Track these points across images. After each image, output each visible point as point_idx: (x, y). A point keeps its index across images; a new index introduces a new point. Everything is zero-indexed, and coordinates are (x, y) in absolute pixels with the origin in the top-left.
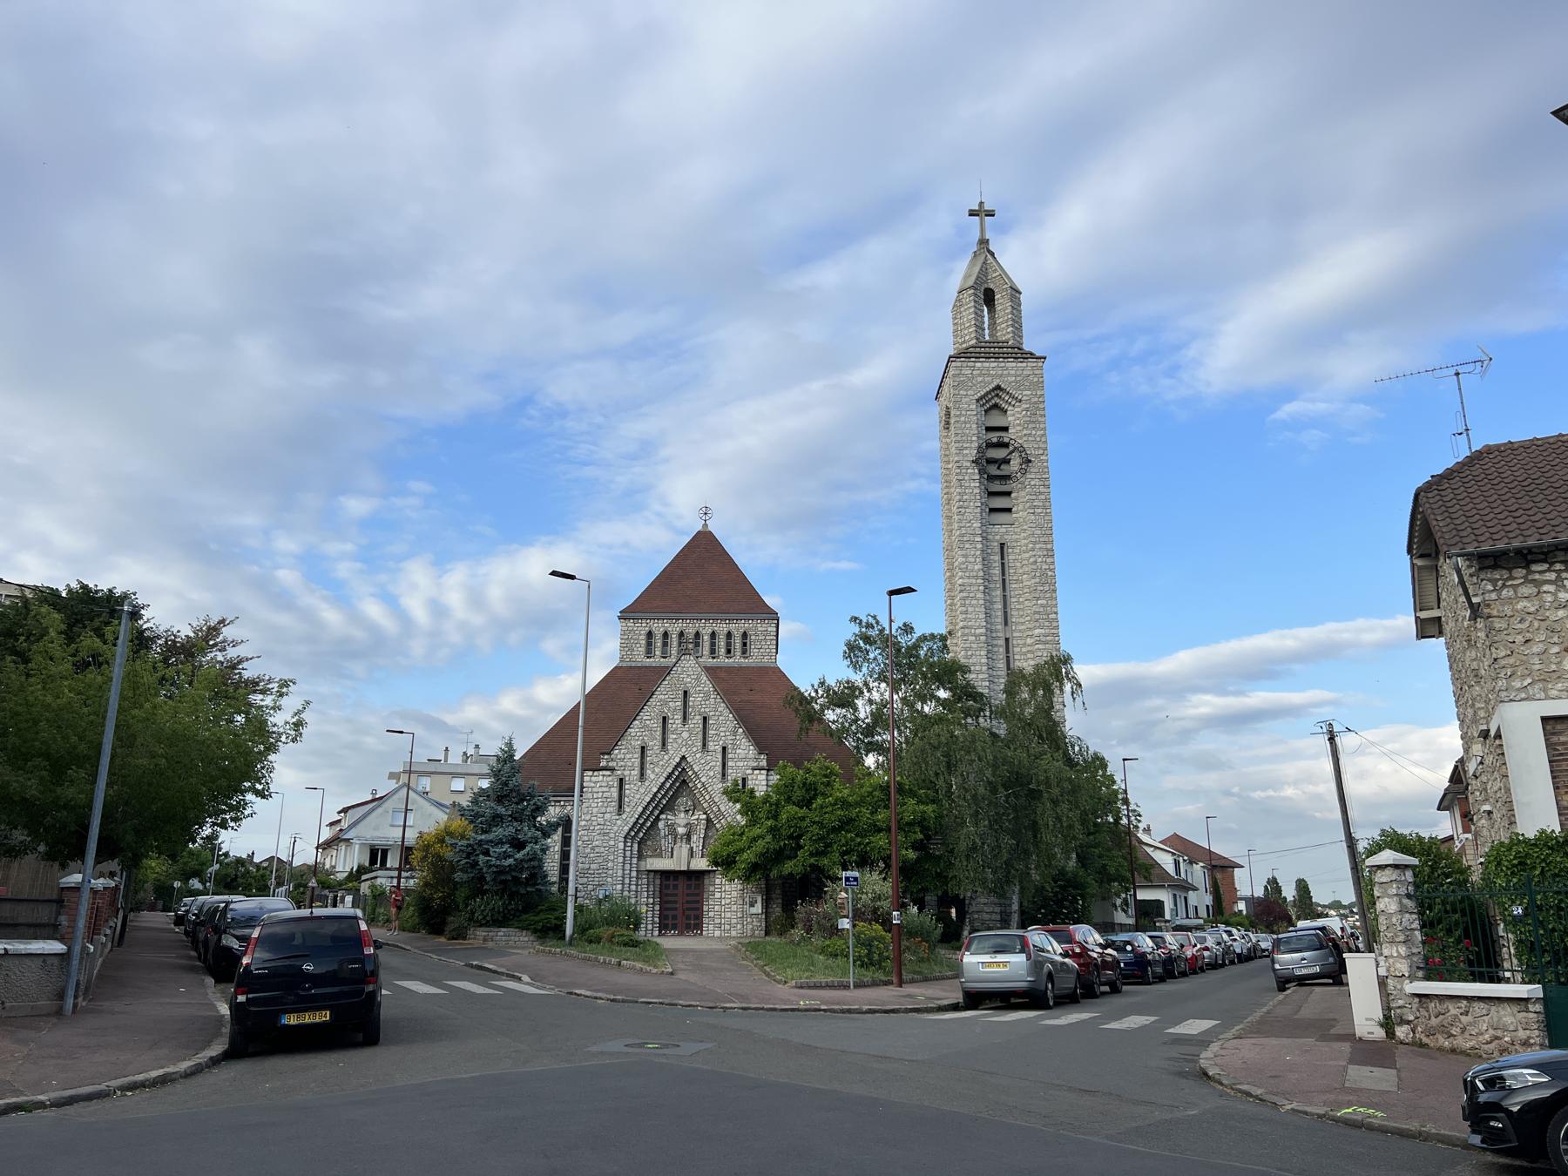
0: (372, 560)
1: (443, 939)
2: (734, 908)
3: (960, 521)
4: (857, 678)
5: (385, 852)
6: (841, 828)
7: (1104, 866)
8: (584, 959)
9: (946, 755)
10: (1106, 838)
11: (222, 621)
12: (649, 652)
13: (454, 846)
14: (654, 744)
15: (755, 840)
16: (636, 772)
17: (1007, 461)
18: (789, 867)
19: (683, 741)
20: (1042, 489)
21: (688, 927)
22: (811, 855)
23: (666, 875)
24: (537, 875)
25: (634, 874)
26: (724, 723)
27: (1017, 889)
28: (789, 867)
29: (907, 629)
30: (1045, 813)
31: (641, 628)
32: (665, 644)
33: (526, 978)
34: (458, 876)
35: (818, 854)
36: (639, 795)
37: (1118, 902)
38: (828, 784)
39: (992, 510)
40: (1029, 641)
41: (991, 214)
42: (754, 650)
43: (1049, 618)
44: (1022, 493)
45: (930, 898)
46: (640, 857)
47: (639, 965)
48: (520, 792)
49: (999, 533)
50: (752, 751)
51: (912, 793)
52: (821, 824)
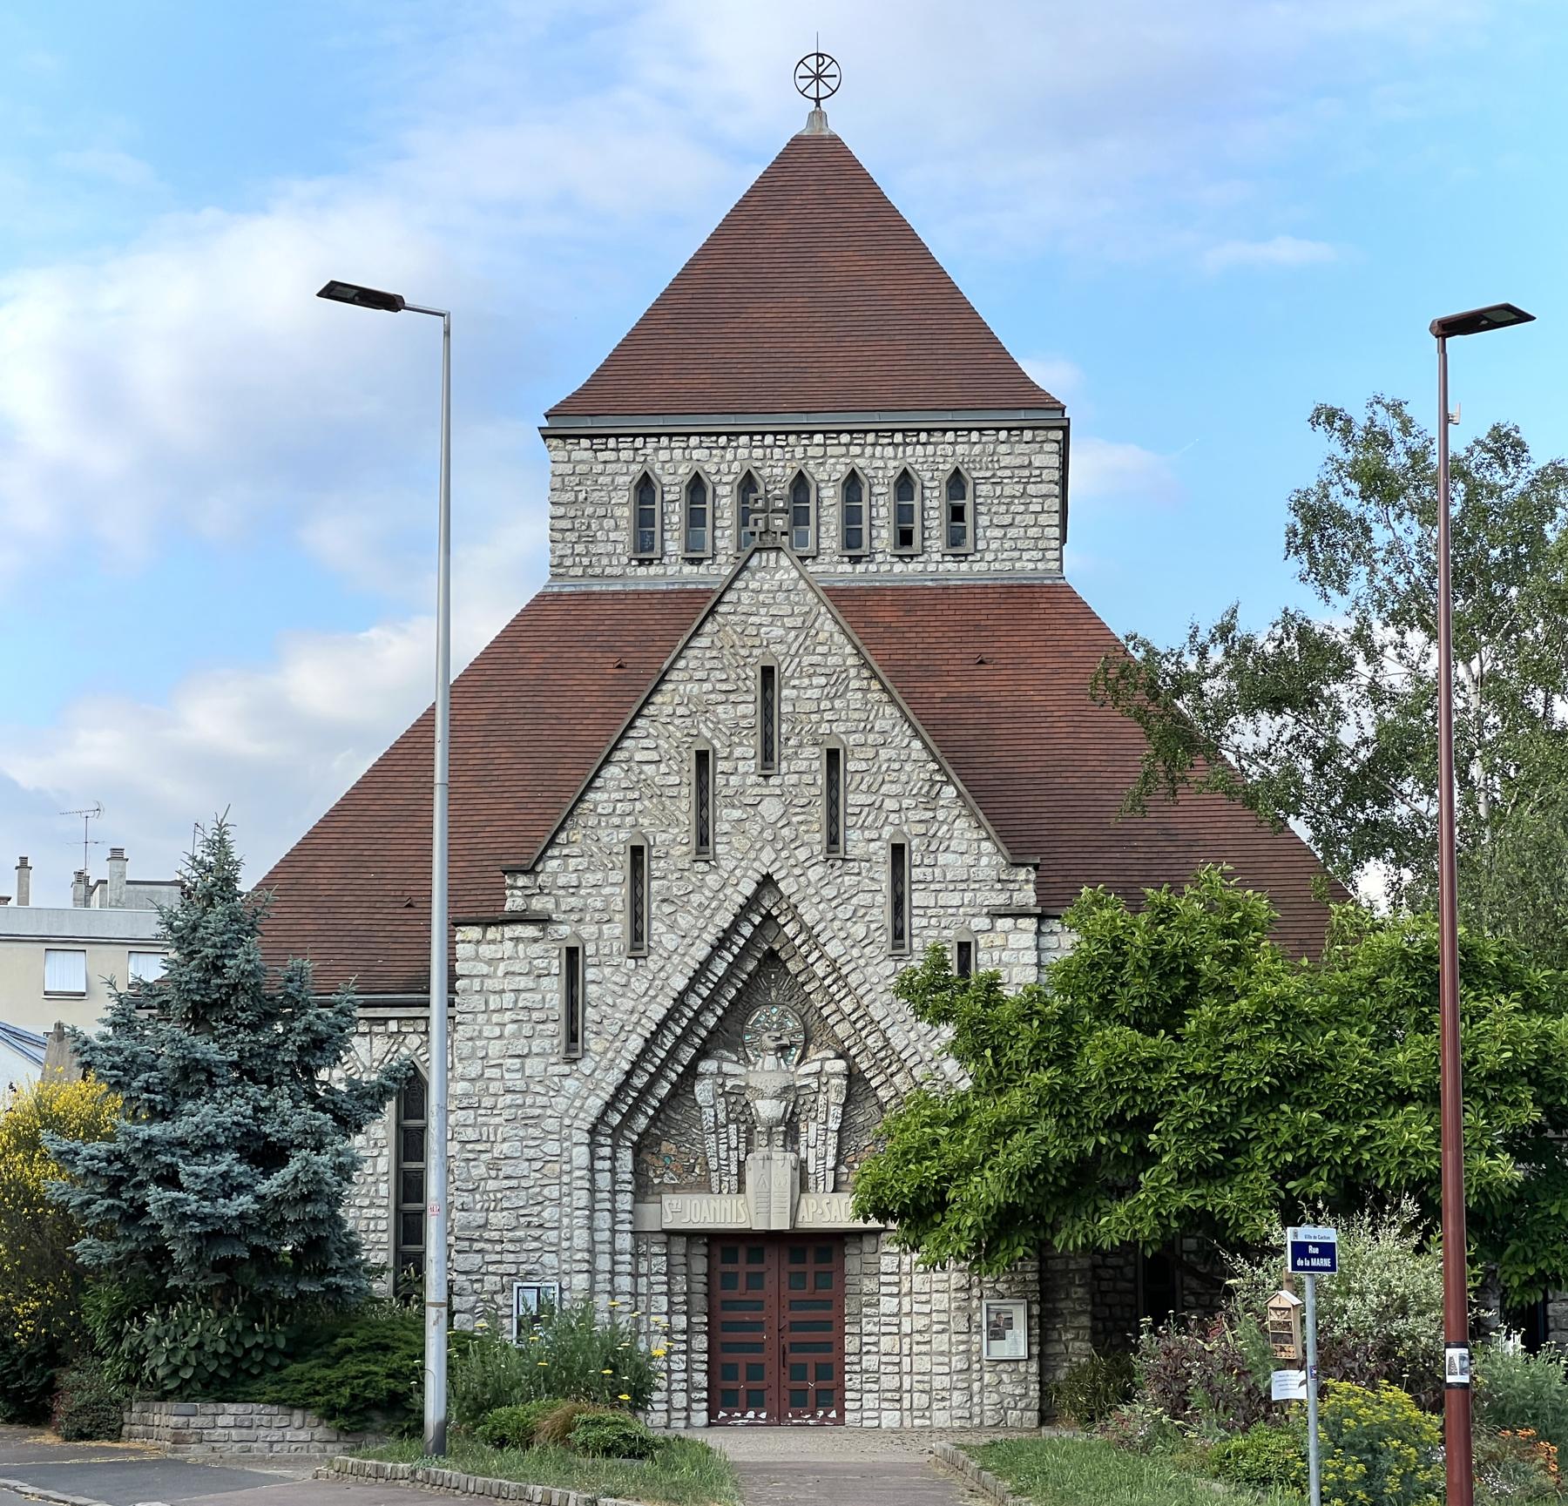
14: (672, 841)
29: (1505, 446)
42: (986, 530)
51: (1506, 980)
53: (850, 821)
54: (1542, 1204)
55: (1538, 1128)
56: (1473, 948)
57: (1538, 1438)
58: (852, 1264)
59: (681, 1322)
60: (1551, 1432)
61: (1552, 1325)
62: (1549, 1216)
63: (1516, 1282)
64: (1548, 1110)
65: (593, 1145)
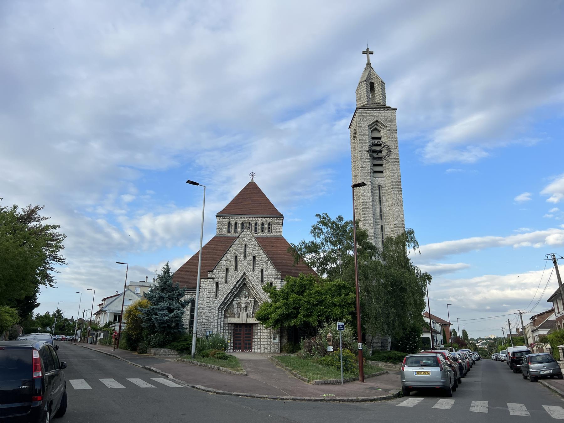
0: (131, 216)
1: (136, 353)
2: (266, 340)
3: (362, 176)
4: (318, 241)
5: (120, 317)
6: (318, 304)
8: (200, 365)
11: (37, 208)
12: (229, 231)
13: (141, 311)
14: (232, 268)
15: (277, 308)
16: (224, 280)
17: (381, 152)
18: (293, 322)
19: (244, 267)
20: (396, 163)
21: (246, 348)
22: (304, 316)
23: (236, 325)
24: (179, 324)
25: (222, 325)
26: (262, 259)
28: (293, 322)
31: (226, 221)
32: (236, 228)
33: (171, 376)
34: (143, 325)
35: (307, 316)
36: (225, 290)
38: (311, 284)
39: (375, 172)
40: (391, 226)
41: (372, 53)
42: (273, 230)
43: (400, 217)
44: (388, 165)
46: (225, 317)
47: (229, 370)
48: (171, 289)
49: (378, 181)
50: (274, 271)
52: (308, 303)
58: (254, 328)
59: (230, 336)
65: (219, 310)
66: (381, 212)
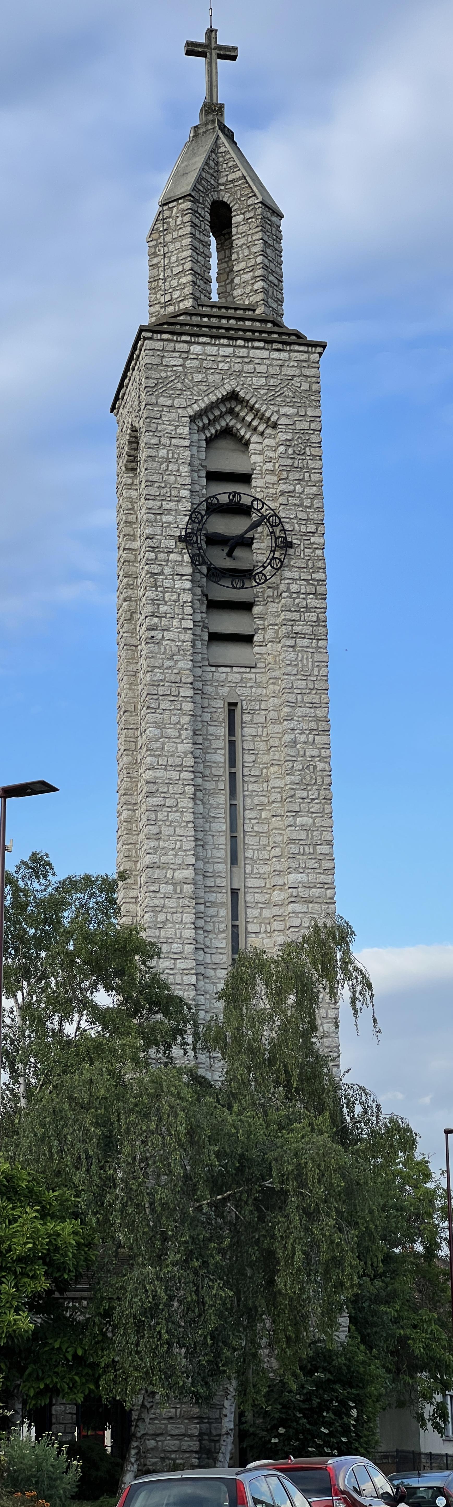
3: (152, 656)
7: (403, 1341)
9: (102, 1122)
10: (408, 1285)
17: (246, 542)
20: (312, 602)
27: (232, 1386)
29: (39, 865)
30: (290, 1234)
37: (428, 1410)
39: (216, 638)
40: (277, 896)
41: (229, 54)
43: (316, 853)
44: (273, 607)
45: (63, 1409)
49: (227, 682)
51: (32, 1196)
53: (249, 814)
54: (50, 1341)
55: (49, 1292)
56: (13, 1177)
57: (38, 1498)
60: (46, 1493)
61: (54, 1420)
62: (53, 1349)
63: (32, 1393)
64: (55, 1280)
66: (233, 826)
